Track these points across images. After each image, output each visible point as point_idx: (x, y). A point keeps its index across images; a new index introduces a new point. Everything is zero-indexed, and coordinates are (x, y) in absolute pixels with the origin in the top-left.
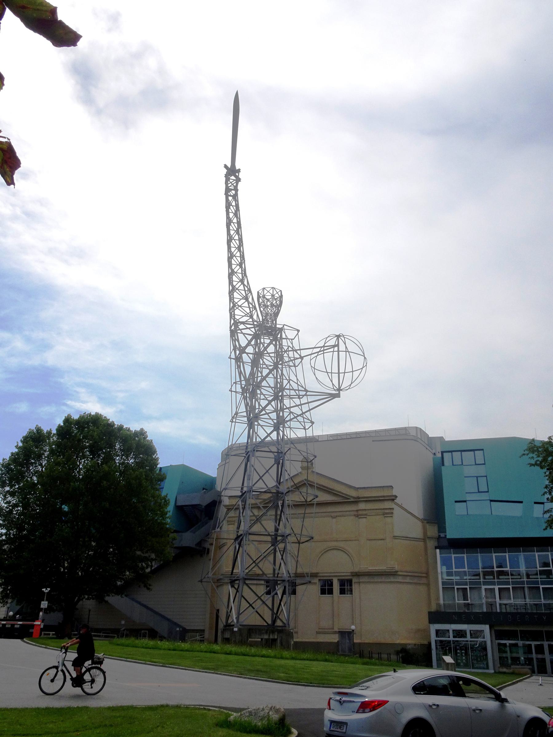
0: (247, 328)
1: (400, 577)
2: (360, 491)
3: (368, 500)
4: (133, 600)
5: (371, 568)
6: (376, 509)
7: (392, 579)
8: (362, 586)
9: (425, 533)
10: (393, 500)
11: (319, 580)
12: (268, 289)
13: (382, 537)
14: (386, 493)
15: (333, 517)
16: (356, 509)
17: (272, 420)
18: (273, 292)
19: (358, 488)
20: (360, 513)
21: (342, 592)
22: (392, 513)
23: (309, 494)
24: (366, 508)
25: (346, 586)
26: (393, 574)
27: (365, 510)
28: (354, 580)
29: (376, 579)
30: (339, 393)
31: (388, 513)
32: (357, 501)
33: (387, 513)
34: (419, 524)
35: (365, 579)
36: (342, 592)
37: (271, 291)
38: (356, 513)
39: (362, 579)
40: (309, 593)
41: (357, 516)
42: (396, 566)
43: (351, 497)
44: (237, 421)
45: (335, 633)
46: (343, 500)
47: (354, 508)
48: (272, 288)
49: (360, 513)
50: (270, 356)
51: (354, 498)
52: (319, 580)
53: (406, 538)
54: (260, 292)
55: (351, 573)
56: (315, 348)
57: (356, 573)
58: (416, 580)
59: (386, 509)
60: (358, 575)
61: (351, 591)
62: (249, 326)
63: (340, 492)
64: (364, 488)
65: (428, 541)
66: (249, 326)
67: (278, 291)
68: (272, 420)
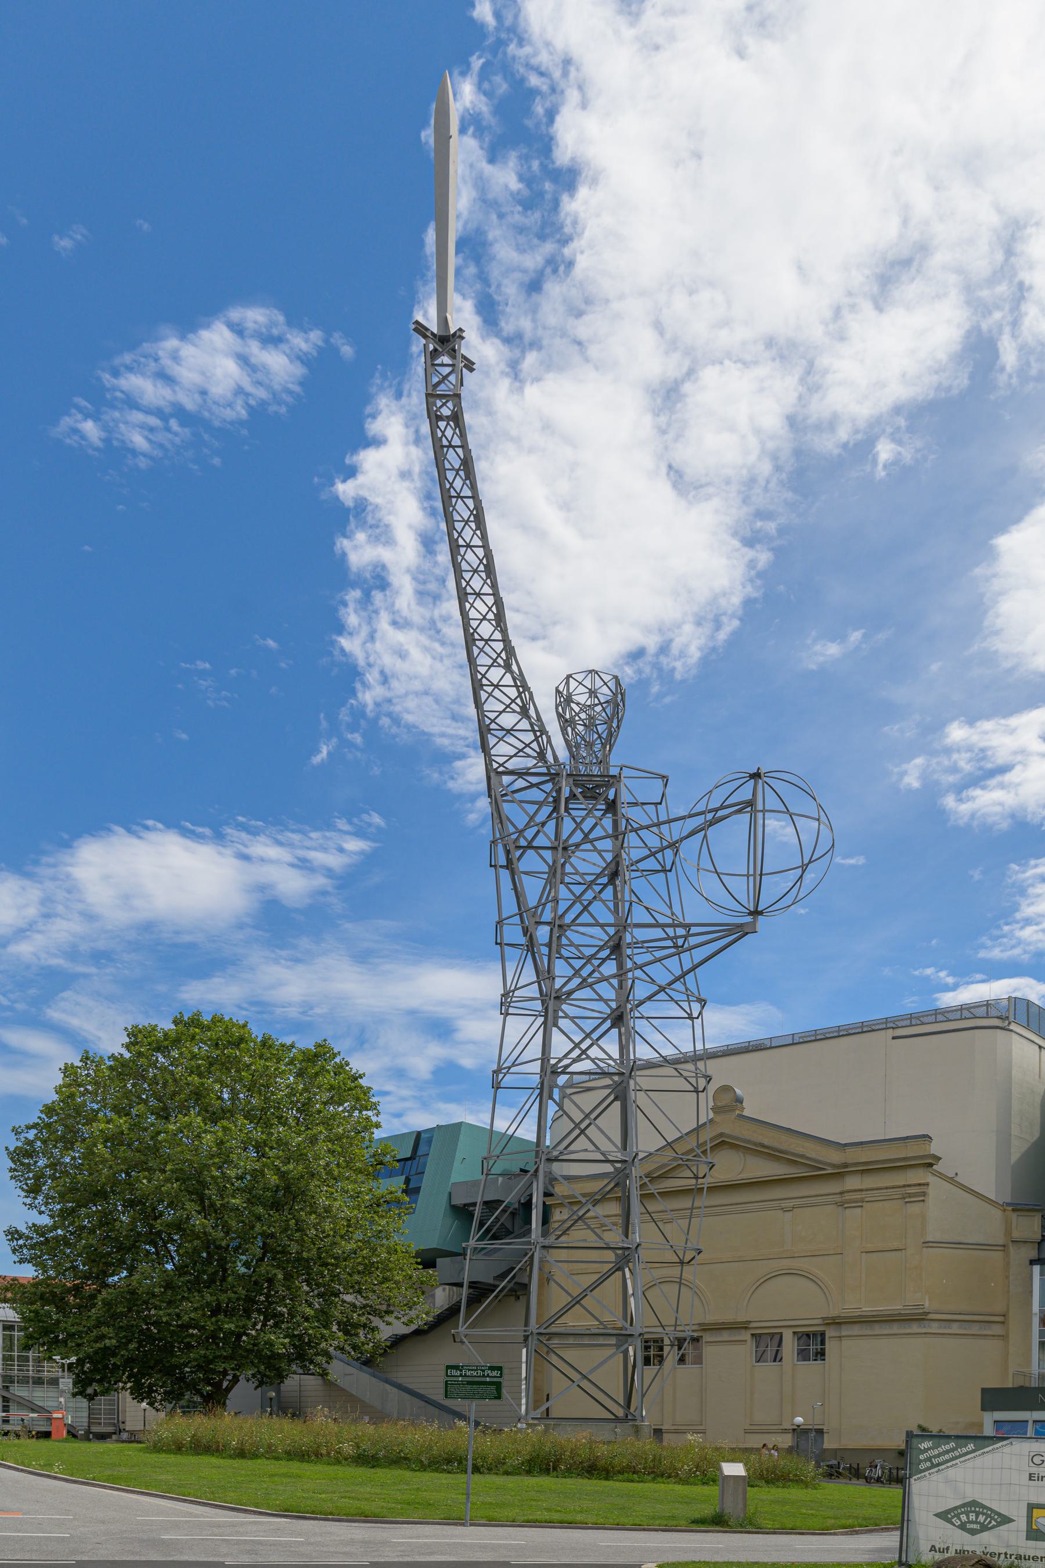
0: (532, 786)
1: (935, 1325)
2: (849, 1150)
3: (867, 1169)
4: (387, 1381)
5: (867, 1309)
6: (887, 1188)
7: (915, 1328)
8: (846, 1343)
9: (1008, 1231)
10: (931, 1165)
11: (752, 1335)
12: (580, 677)
13: (896, 1245)
14: (913, 1150)
15: (785, 1210)
16: (838, 1191)
17: (606, 1001)
18: (593, 682)
19: (846, 1145)
20: (848, 1197)
21: (803, 1355)
22: (924, 1194)
23: (729, 1167)
24: (864, 1187)
25: (813, 1345)
26: (919, 1317)
27: (861, 1190)
28: (830, 1333)
29: (877, 1329)
30: (754, 923)
31: (919, 1194)
32: (840, 1173)
33: (910, 1195)
34: (997, 1213)
35: (856, 1330)
36: (803, 1355)
37: (588, 683)
38: (837, 1198)
39: (845, 1331)
40: (728, 1360)
41: (841, 1204)
42: (927, 1304)
43: (829, 1164)
44: (511, 1010)
45: (785, 1431)
46: (807, 1169)
47: (833, 1187)
48: (590, 672)
49: (848, 1197)
50: (595, 849)
51: (834, 1166)
52: (752, 1335)
53: (958, 1244)
54: (561, 689)
55: (823, 1319)
56: (690, 816)
57: (833, 1318)
58: (975, 1329)
59: (909, 1186)
60: (836, 1322)
61: (698, 1360)
62: (534, 780)
63: (802, 1156)
64: (861, 1143)
65: (1012, 1249)
66: (534, 780)
67: (607, 678)
68: (606, 1001)
